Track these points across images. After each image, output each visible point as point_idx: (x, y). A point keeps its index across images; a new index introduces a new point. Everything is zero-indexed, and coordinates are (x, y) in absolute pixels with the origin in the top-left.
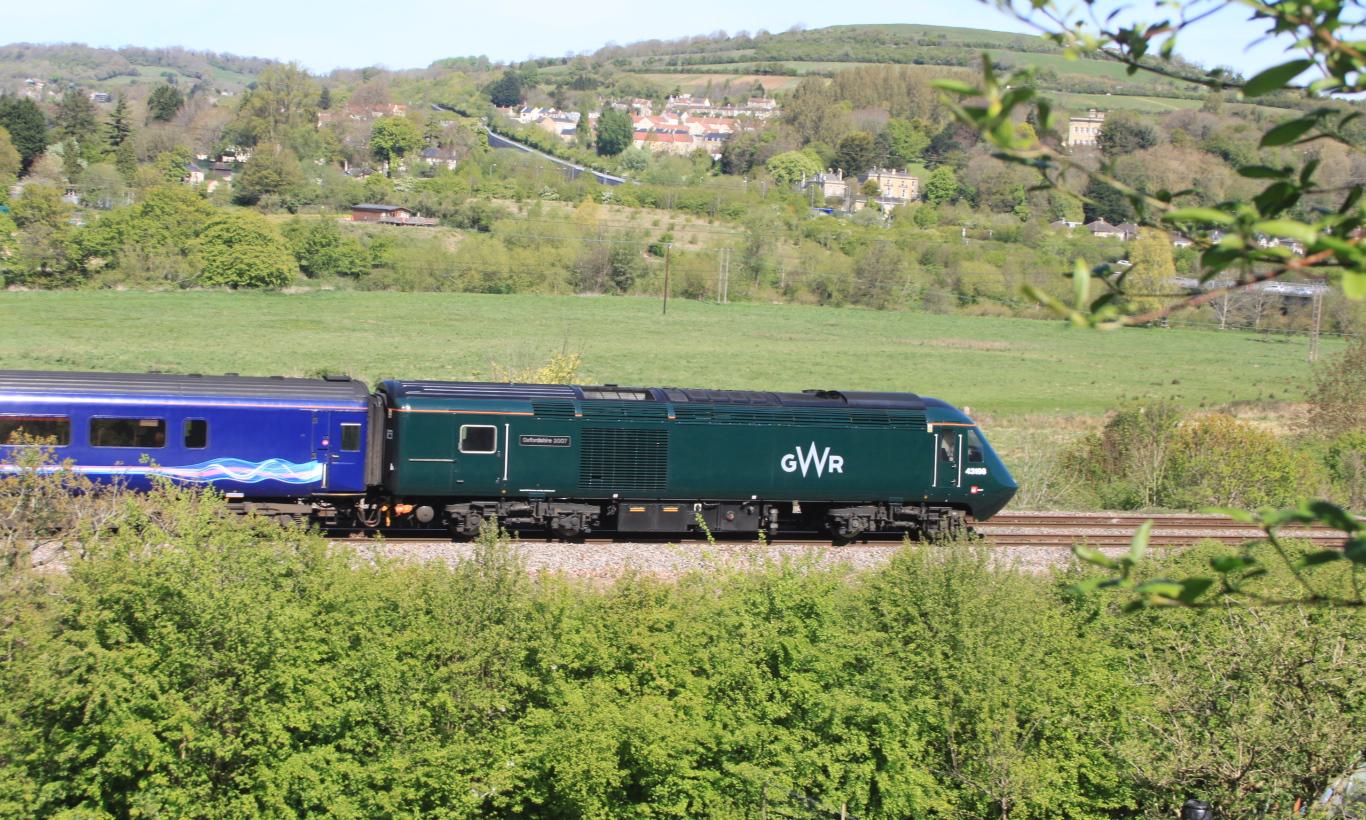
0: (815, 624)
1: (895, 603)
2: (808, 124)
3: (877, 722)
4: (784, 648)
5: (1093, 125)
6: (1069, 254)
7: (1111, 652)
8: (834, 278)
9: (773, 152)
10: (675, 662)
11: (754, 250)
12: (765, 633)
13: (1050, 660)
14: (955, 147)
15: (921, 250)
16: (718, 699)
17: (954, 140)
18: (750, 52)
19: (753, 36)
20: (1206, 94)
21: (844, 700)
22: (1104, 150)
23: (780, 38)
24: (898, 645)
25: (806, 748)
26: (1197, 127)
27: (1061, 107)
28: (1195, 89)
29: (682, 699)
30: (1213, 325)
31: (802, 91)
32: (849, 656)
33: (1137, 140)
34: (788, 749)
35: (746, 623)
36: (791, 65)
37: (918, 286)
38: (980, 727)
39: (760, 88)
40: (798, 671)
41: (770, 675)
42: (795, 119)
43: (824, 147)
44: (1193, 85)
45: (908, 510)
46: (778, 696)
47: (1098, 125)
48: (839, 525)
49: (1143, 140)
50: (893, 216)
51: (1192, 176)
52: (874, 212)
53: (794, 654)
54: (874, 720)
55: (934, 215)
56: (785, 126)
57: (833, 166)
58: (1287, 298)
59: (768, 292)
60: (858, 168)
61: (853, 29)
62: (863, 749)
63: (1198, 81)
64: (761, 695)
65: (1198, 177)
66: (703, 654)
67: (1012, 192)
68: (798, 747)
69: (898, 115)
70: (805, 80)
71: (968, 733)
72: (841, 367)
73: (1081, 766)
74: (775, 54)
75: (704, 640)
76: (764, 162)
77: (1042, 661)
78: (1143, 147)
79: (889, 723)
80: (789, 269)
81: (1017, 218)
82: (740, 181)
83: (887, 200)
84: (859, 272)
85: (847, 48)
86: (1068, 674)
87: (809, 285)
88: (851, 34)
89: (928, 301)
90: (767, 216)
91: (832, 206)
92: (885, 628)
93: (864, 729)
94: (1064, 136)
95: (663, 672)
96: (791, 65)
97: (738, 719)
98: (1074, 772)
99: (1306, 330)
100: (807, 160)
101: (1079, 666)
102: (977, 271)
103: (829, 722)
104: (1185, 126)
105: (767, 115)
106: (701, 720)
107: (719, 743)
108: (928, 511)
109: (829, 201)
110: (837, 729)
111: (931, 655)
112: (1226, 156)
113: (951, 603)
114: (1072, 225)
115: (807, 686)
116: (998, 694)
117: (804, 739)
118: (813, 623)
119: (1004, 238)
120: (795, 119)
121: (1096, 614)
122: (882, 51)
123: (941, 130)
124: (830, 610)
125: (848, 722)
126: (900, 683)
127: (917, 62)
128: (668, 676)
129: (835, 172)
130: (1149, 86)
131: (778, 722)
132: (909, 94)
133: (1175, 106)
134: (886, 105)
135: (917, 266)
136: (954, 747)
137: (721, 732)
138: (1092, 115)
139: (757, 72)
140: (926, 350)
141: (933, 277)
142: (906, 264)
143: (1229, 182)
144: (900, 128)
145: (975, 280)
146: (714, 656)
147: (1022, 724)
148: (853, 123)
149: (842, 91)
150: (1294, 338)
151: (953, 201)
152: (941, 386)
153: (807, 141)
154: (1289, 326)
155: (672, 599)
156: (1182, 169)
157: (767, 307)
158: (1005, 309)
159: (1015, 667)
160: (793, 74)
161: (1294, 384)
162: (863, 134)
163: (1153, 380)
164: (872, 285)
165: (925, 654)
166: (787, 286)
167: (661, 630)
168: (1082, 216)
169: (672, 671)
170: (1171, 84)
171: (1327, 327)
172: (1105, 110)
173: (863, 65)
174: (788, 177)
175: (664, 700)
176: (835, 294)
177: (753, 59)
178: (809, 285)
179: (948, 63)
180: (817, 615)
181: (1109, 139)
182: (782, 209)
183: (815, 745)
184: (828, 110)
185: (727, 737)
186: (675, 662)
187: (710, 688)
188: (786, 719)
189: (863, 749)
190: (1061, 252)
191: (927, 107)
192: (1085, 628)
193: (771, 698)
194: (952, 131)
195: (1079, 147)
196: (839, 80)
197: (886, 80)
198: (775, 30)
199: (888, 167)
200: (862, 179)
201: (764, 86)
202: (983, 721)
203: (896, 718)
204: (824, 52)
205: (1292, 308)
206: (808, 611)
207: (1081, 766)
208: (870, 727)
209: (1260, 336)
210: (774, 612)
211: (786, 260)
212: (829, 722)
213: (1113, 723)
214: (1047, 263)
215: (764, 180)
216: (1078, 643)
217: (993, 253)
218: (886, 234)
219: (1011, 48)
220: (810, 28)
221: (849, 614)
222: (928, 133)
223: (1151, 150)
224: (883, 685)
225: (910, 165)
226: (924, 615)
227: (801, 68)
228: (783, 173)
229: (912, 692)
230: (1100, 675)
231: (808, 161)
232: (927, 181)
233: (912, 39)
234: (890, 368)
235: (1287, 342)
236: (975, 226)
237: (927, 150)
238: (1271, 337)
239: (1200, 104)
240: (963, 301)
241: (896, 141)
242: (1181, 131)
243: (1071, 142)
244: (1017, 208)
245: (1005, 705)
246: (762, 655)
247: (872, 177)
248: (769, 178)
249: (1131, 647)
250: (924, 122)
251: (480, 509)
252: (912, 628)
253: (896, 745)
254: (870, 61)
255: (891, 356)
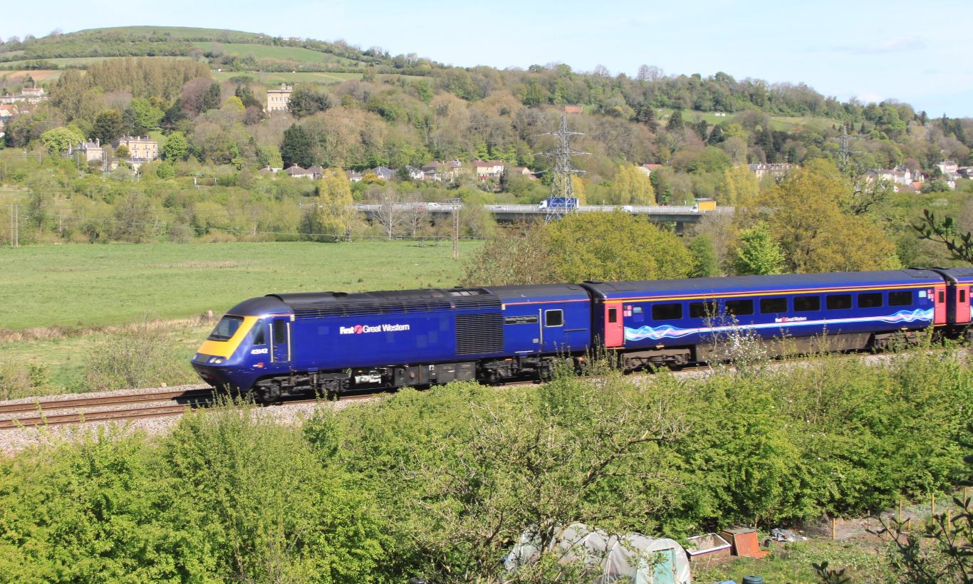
0: (127, 477)
1: (185, 456)
2: (70, 105)
3: (180, 546)
4: (106, 497)
5: (284, 95)
6: (274, 192)
7: (347, 476)
8: (100, 221)
9: (44, 128)
10: (22, 517)
11: (37, 203)
12: (89, 488)
13: (304, 486)
14: (184, 117)
15: (165, 196)
16: (56, 542)
17: (183, 111)
18: (21, 53)
19: (22, 40)
20: (364, 68)
21: (153, 532)
22: (294, 113)
23: (44, 41)
24: (191, 488)
25: (127, 573)
26: (360, 92)
27: (260, 83)
28: (356, 65)
29: (30, 544)
30: (383, 237)
31: (63, 80)
32: (154, 498)
33: (317, 104)
34: (114, 575)
35: (73, 482)
36: (54, 61)
37: (164, 223)
38: (258, 541)
39: (31, 80)
40: (117, 514)
41: (95, 520)
42: (60, 102)
43: (84, 123)
44: (354, 62)
45: (530, 361)
46: (103, 535)
47: (288, 95)
48: (264, 392)
49: (322, 104)
50: (140, 172)
51: (359, 129)
52: (126, 170)
53: (114, 501)
54: (177, 545)
55: (172, 169)
56: (52, 108)
57: (92, 136)
58: (434, 213)
59: (50, 236)
60: (111, 137)
61: (99, 31)
62: (171, 568)
63: (357, 59)
64: (90, 535)
65: (363, 129)
66: (42, 509)
67: (229, 149)
68: (121, 572)
69: (139, 95)
70: (65, 72)
71: (248, 548)
72: (113, 289)
73: (333, 562)
74: (40, 54)
75: (42, 497)
76: (38, 137)
77: (298, 488)
78: (322, 109)
79: (188, 545)
80: (65, 216)
81: (234, 167)
82: (20, 153)
83: (135, 160)
84: (119, 216)
85: (96, 46)
86: (318, 495)
87: (81, 229)
88: (97, 35)
89: (172, 234)
90: (45, 179)
91: (93, 167)
92: (180, 475)
93: (170, 553)
94: (264, 105)
95: (12, 526)
96: (54, 61)
97: (73, 556)
98: (328, 568)
99: (448, 237)
100: (71, 133)
101: (326, 489)
102: (207, 209)
103: (143, 550)
104: (351, 92)
105: (38, 100)
106: (44, 560)
107: (60, 576)
108: (541, 360)
109: (91, 163)
110: (150, 555)
111: (217, 492)
112: (382, 113)
113: (227, 451)
114: (275, 170)
115: (125, 524)
116: (269, 514)
117: (125, 565)
118: (125, 476)
119: (225, 183)
120: (60, 102)
121: (335, 449)
122: (122, 47)
123: (172, 105)
124: (137, 465)
125: (158, 549)
126: (195, 515)
127: (150, 55)
128: (16, 529)
129: (94, 141)
130: (323, 65)
131: (105, 554)
132: (145, 78)
133: (343, 78)
134: (128, 88)
135: (162, 208)
136: (240, 558)
137: (61, 567)
138: (283, 88)
139: (27, 68)
140: (174, 271)
141: (175, 216)
142: (154, 207)
143: (386, 132)
144: (141, 105)
145: (207, 216)
146: (50, 510)
147: (288, 536)
148: (106, 103)
149: (96, 78)
150: (441, 243)
151: (185, 158)
152: (189, 297)
153: (70, 119)
154: (437, 234)
155: (16, 468)
156: (352, 124)
157: (50, 248)
158: (231, 236)
159: (279, 494)
160: (55, 68)
161: (444, 275)
162: (113, 111)
163: (344, 280)
164: (129, 225)
165: (211, 491)
166: (64, 230)
167: (8, 494)
168: (282, 163)
169: (19, 525)
170: (338, 62)
171: (463, 232)
172: (293, 84)
173: (108, 59)
174: (58, 148)
175: (14, 548)
176: (101, 234)
177: (23, 58)
178: (81, 229)
179: (173, 54)
180: (127, 469)
181: (297, 105)
182: (56, 172)
183: (134, 569)
184: (85, 94)
185: (66, 571)
186: (22, 517)
187: (50, 535)
188: (111, 552)
189: (171, 568)
190: (268, 191)
191: (160, 89)
192: (328, 461)
193: (98, 536)
194: (180, 105)
195: (275, 112)
196: (92, 71)
197: (127, 69)
198: (38, 36)
199: (134, 135)
200: (115, 146)
201: (33, 79)
202: (259, 536)
203: (194, 541)
204: (78, 50)
205: (438, 221)
206: (119, 467)
207: (333, 562)
208: (175, 551)
209: (417, 243)
210: (94, 472)
211: (61, 211)
212: (143, 550)
213: (353, 528)
214: (259, 199)
215: (40, 150)
216: (324, 472)
217: (218, 195)
218: (137, 185)
219: (219, 41)
220: (66, 32)
221: (151, 467)
222: (162, 108)
223: (327, 111)
224: (182, 518)
225: (151, 133)
226: (208, 462)
227: (62, 63)
228: (53, 144)
229: (204, 521)
230: (341, 494)
231: (72, 134)
232: (164, 144)
233: (144, 38)
234: (150, 286)
235: (436, 246)
236: (203, 176)
237: (163, 121)
238: (424, 243)
239: (361, 76)
240: (199, 233)
241: (139, 115)
242: (349, 97)
243: (270, 109)
244: (233, 160)
245: (275, 523)
246: (88, 505)
247: (122, 143)
248: (43, 148)
249: (361, 471)
250: (159, 99)
251: (279, 382)
252: (200, 473)
253: (196, 562)
254: (114, 55)
255: (149, 278)
